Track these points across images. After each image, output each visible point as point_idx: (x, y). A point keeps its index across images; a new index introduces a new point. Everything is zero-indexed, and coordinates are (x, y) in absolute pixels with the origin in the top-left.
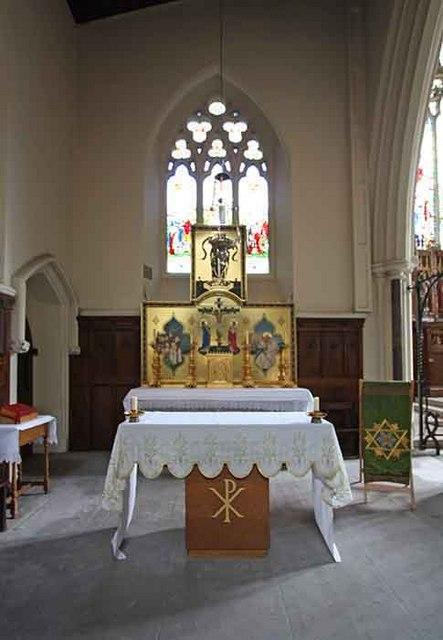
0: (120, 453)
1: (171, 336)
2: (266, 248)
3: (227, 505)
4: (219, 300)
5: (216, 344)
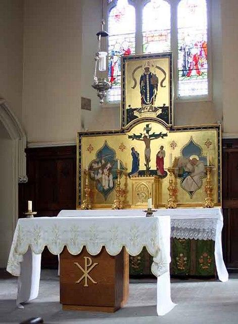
0: (18, 237)
1: (103, 161)
2: (204, 70)
3: (86, 275)
4: (147, 126)
5: (145, 169)
